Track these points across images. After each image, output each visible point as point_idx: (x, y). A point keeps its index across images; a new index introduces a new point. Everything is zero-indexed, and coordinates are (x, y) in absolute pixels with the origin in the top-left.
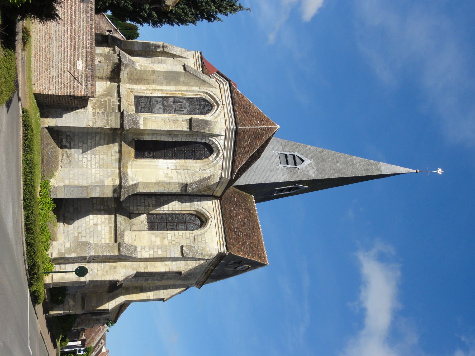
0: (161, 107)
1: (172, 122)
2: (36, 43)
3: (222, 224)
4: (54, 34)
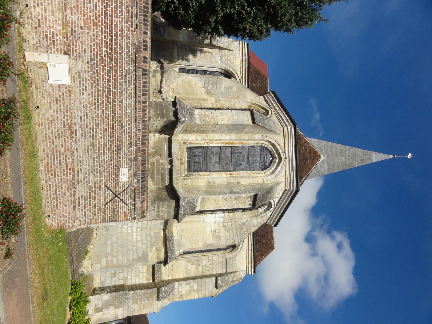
0: (218, 160)
2: (47, 145)
3: (252, 246)
4: (79, 124)
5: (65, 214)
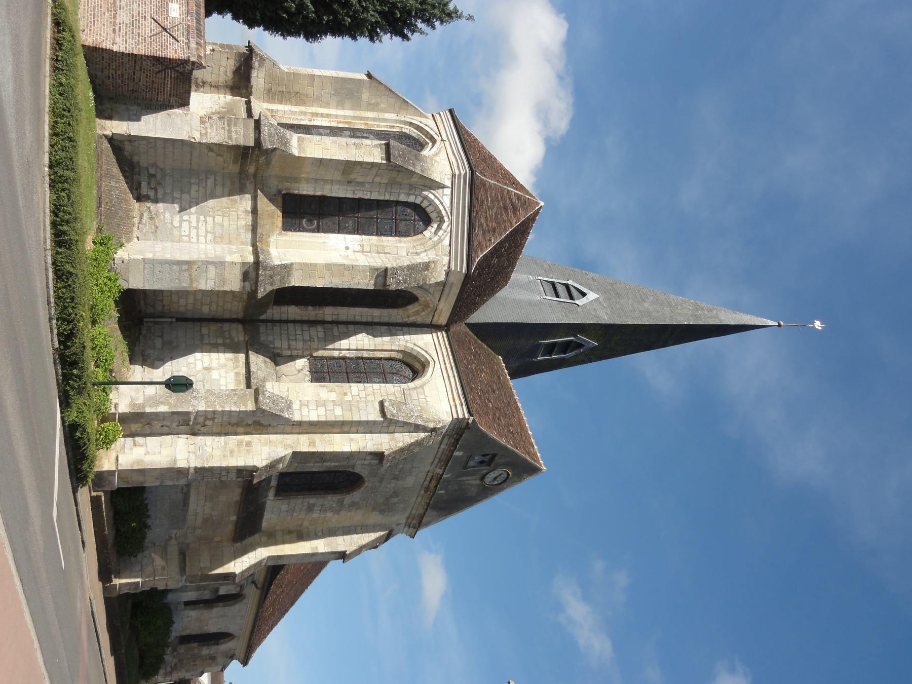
1: (353, 147)
3: (454, 370)
5: (102, 33)
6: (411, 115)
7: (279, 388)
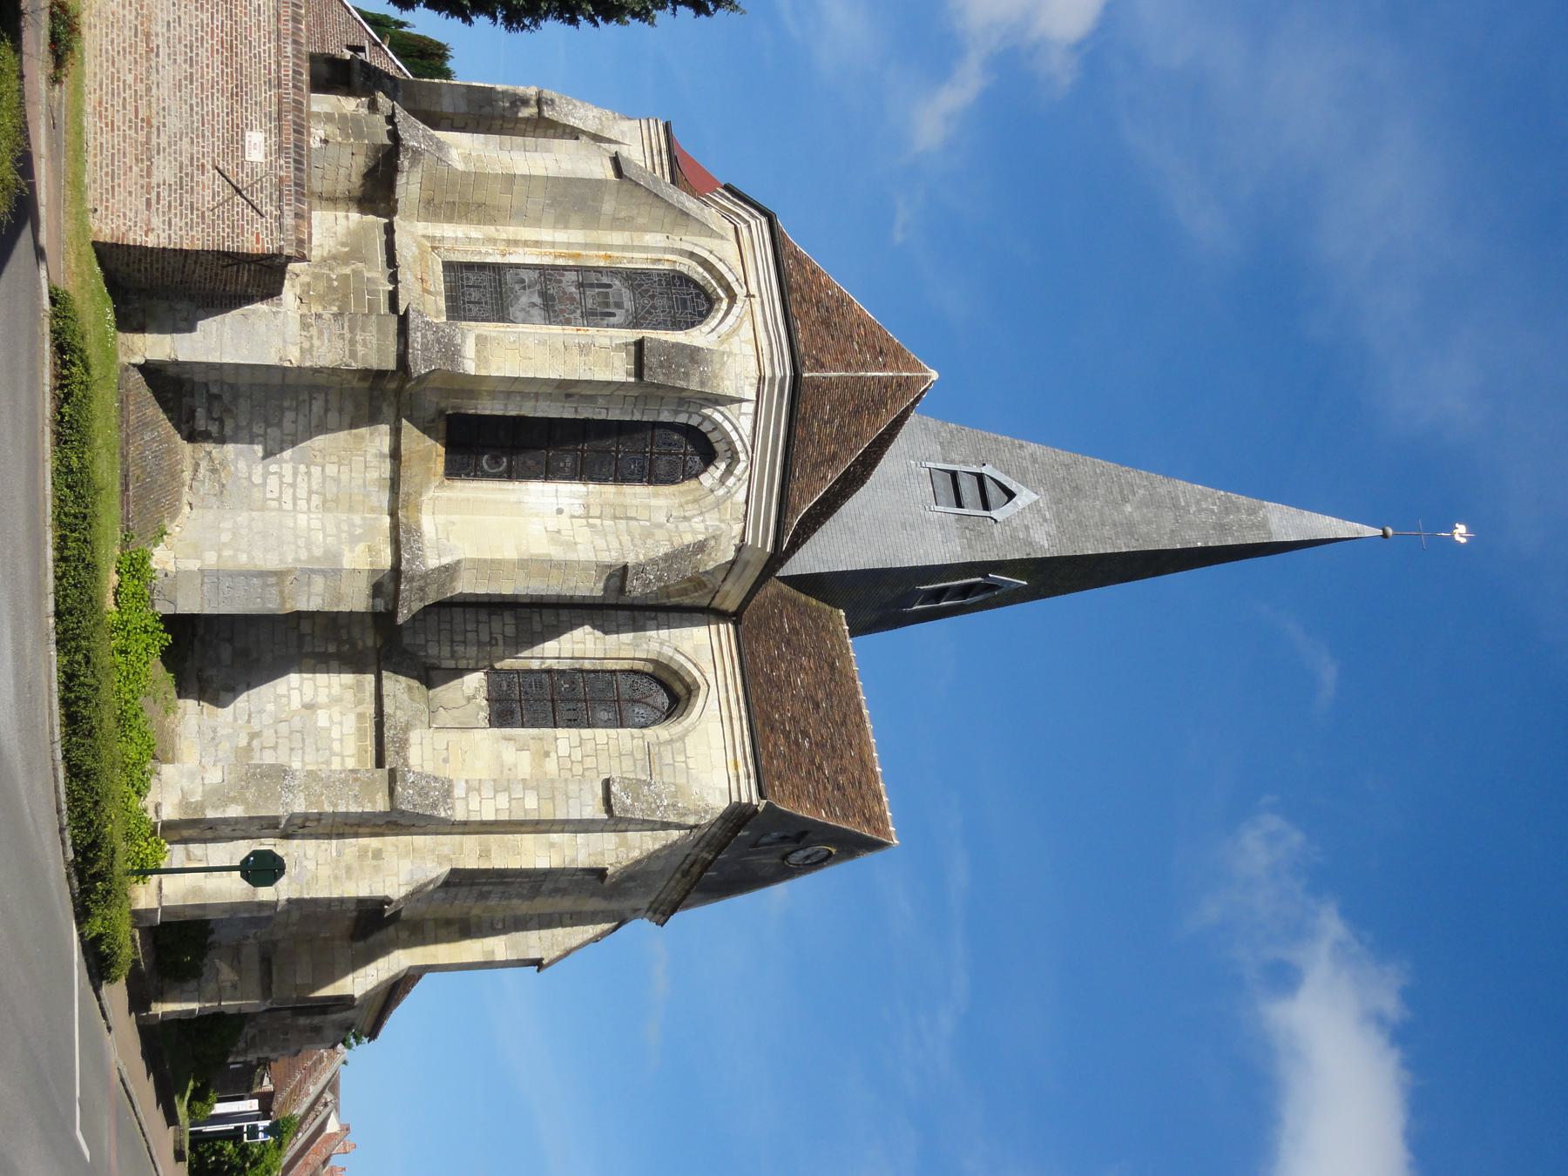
0: (537, 299)
1: (576, 351)
2: (101, 66)
4: (163, 34)
5: (128, 212)
6: (694, 235)
7: (433, 744)
